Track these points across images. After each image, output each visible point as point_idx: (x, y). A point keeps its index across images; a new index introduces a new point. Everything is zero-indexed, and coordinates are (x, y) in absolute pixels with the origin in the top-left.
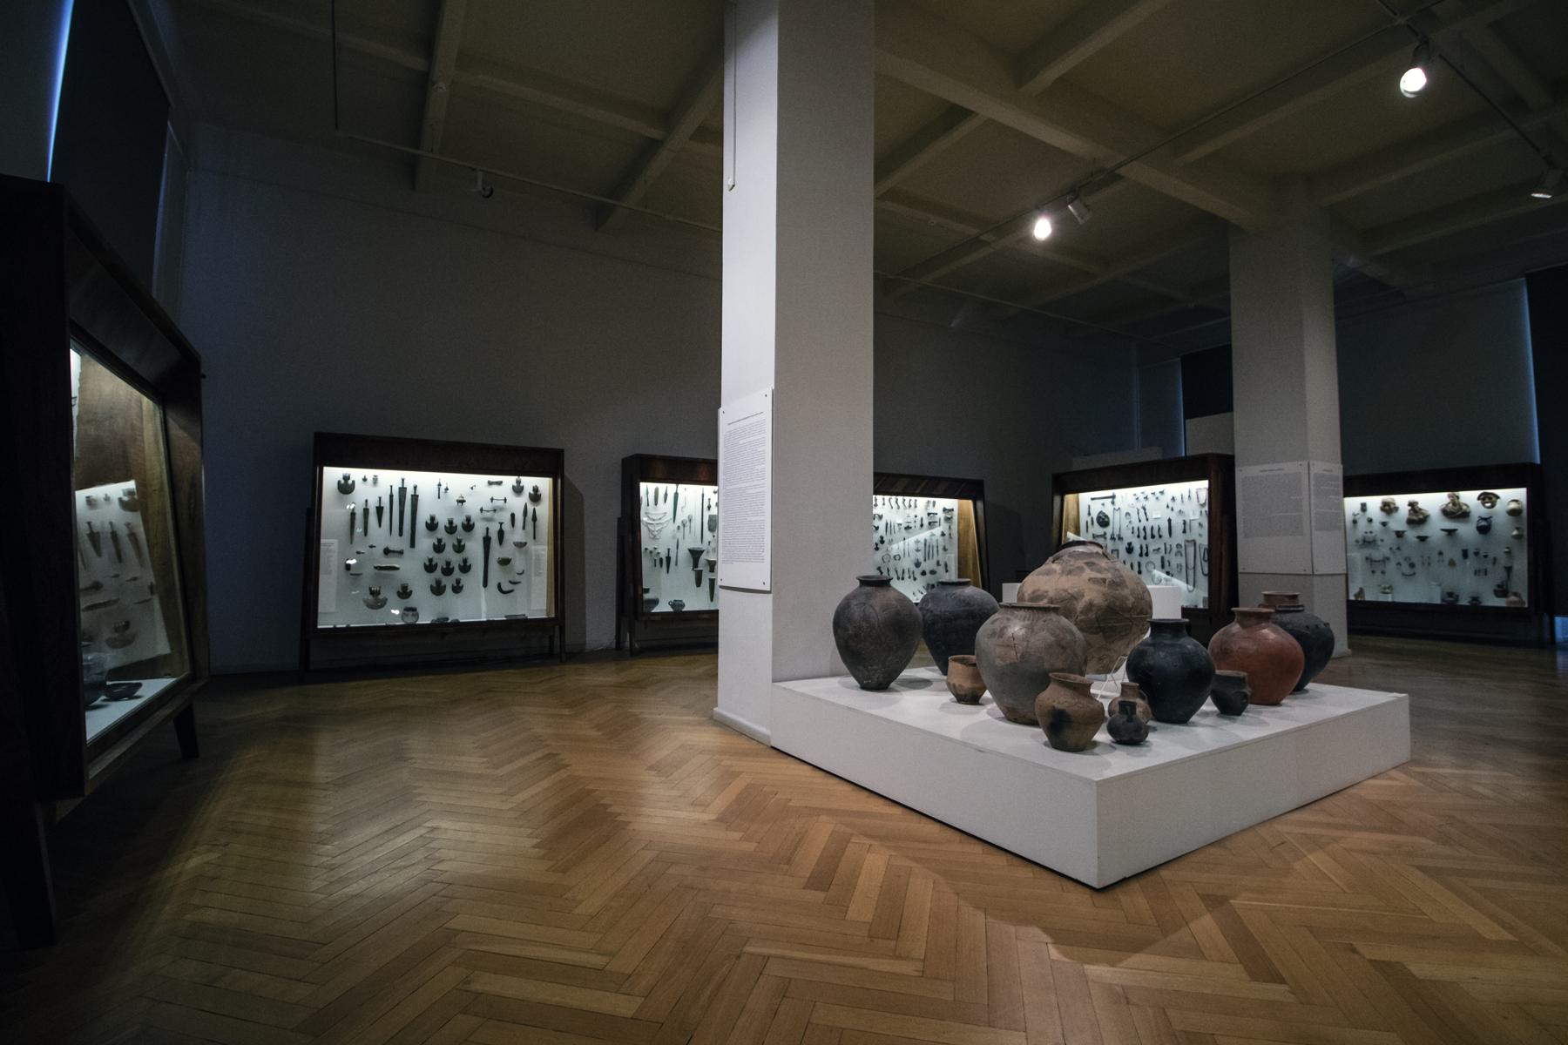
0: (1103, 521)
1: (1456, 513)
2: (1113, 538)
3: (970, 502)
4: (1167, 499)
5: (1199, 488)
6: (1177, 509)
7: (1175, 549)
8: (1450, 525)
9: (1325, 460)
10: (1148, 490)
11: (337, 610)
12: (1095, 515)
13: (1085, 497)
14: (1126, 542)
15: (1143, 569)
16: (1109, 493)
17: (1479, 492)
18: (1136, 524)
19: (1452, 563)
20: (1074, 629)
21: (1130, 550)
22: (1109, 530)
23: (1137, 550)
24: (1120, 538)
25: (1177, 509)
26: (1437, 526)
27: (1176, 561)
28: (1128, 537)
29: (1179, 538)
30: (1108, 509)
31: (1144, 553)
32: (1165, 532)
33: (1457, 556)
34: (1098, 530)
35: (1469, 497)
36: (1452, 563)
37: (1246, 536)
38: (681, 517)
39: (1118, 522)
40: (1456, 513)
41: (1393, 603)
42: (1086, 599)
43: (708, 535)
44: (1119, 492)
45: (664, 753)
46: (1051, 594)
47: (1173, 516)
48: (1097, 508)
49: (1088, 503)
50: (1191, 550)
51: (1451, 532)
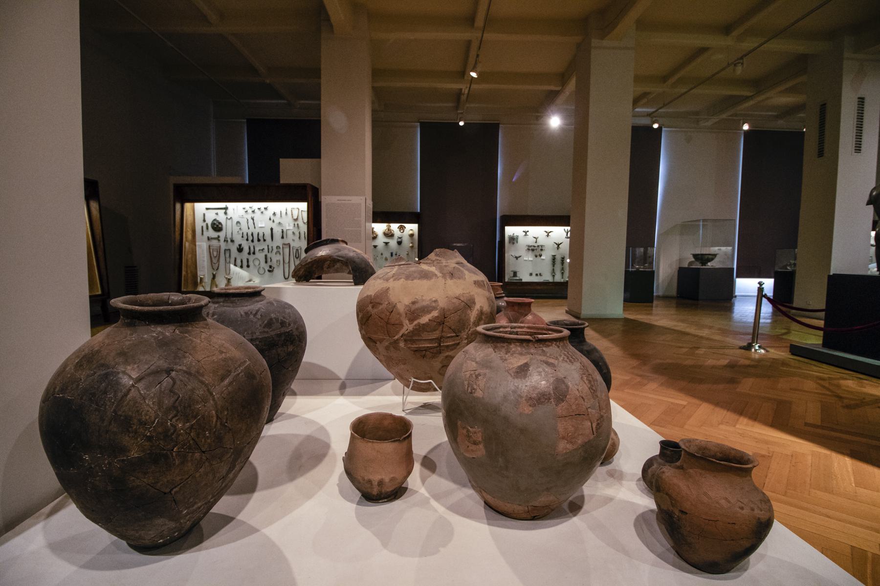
0: (217, 227)
1: (389, 234)
2: (226, 241)
4: (269, 213)
5: (303, 206)
6: (277, 221)
7: (275, 250)
8: (387, 240)
9: (363, 201)
10: (256, 205)
12: (209, 221)
13: (201, 207)
14: (236, 245)
15: (251, 263)
17: (399, 225)
18: (245, 229)
19: (386, 259)
20: (396, 337)
21: (240, 249)
22: (222, 234)
23: (246, 249)
24: (232, 241)
25: (277, 221)
26: (381, 240)
27: (275, 258)
28: (238, 240)
29: (278, 241)
30: (221, 217)
31: (252, 252)
32: (268, 237)
33: (388, 255)
34: (212, 233)
35: (395, 227)
36: (386, 259)
39: (229, 228)
40: (389, 234)
42: (477, 307)
44: (231, 206)
46: (442, 304)
47: (274, 226)
48: (211, 217)
49: (203, 211)
50: (287, 250)
51: (386, 243)
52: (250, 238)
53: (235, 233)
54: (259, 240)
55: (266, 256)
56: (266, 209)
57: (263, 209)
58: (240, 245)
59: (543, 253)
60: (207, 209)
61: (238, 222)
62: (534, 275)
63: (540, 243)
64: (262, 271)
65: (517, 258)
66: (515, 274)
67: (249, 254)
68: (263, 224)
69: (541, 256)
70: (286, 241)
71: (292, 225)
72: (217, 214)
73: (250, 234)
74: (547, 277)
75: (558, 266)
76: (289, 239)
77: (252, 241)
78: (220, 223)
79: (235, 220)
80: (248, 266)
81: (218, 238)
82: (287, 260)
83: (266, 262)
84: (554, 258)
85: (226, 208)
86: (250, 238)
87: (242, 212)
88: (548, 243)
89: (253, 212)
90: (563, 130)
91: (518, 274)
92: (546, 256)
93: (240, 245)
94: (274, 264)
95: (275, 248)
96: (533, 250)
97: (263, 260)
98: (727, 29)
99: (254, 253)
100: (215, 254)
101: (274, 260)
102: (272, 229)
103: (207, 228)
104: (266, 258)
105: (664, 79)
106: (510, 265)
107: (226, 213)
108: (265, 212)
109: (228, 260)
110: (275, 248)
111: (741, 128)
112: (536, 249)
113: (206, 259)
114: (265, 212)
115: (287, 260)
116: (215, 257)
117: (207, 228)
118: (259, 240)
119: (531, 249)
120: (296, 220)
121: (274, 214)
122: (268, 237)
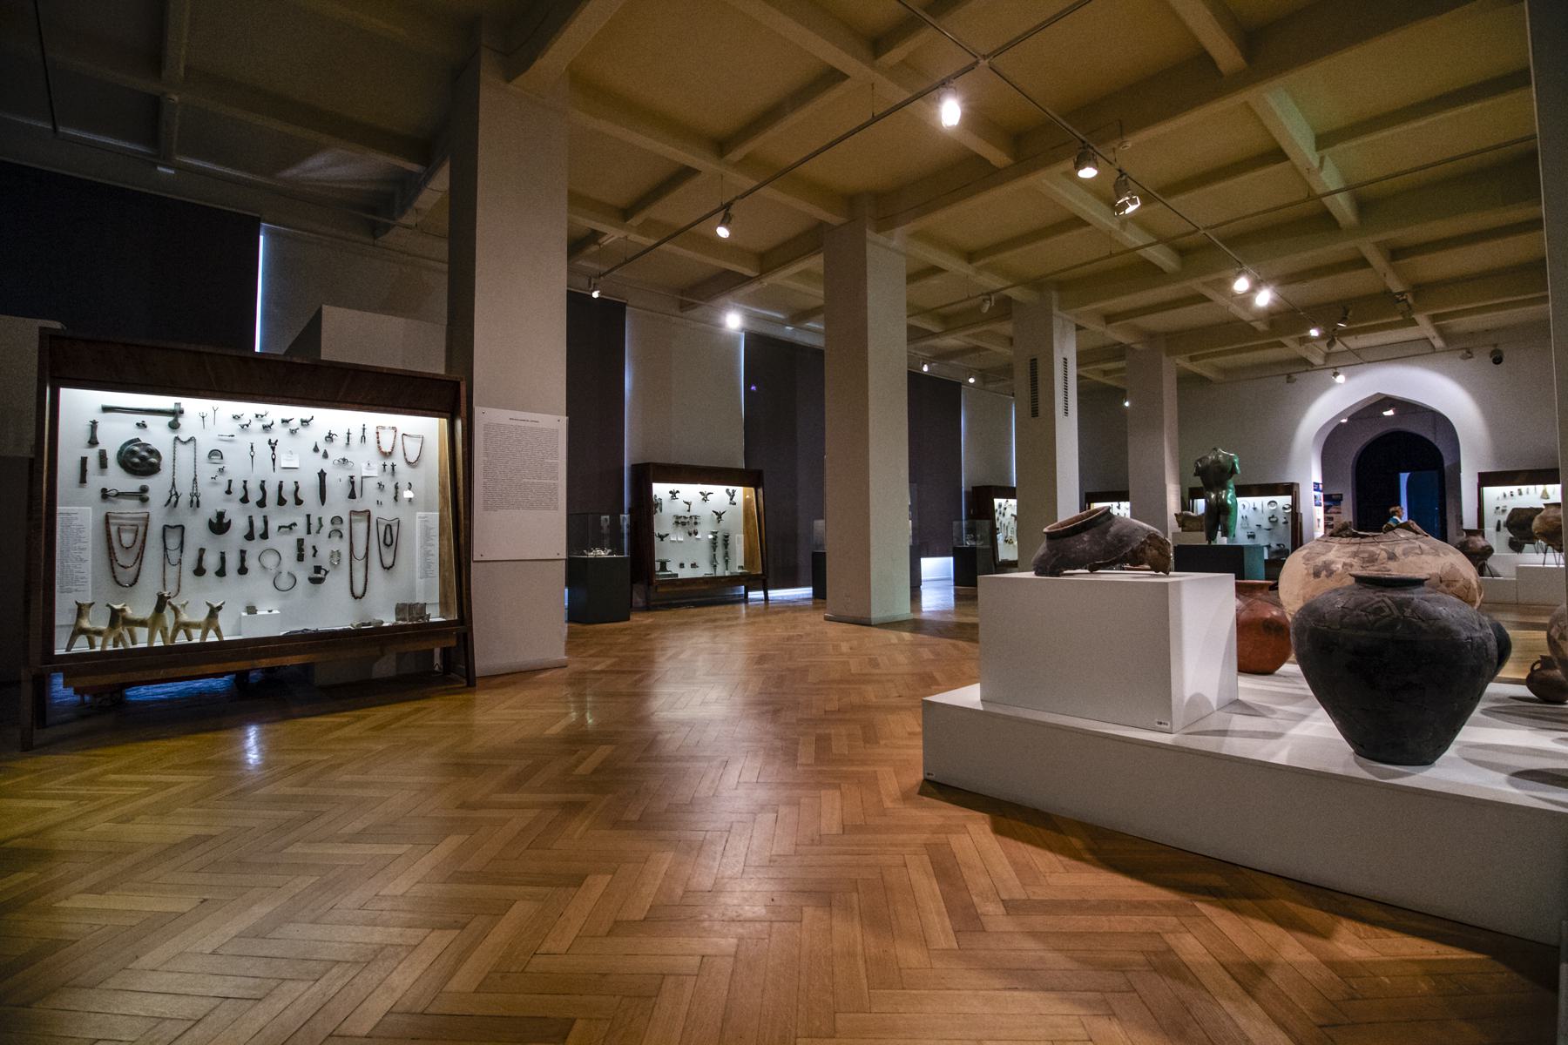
2: (173, 501)
4: (316, 433)
5: (423, 432)
7: (327, 527)
10: (276, 412)
11: (454, 616)
14: (208, 512)
15: (252, 563)
16: (167, 402)
18: (237, 467)
22: (157, 486)
27: (327, 547)
29: (338, 504)
30: (157, 435)
37: (486, 509)
39: (179, 467)
44: (194, 407)
47: (327, 466)
48: (116, 433)
50: (360, 528)
52: (255, 496)
54: (281, 501)
55: (300, 542)
56: (305, 422)
57: (296, 424)
58: (221, 515)
60: (106, 409)
61: (215, 453)
62: (688, 566)
64: (284, 582)
65: (662, 537)
66: (663, 565)
67: (250, 537)
70: (359, 505)
72: (142, 426)
73: (254, 487)
74: (704, 571)
77: (262, 503)
80: (243, 570)
81: (142, 495)
82: (360, 550)
83: (300, 558)
85: (176, 413)
88: (703, 511)
89: (266, 428)
92: (705, 534)
93: (221, 515)
94: (324, 559)
96: (684, 524)
97: (289, 552)
99: (265, 536)
100: (127, 538)
102: (322, 475)
105: (625, 213)
106: (661, 551)
107: (174, 426)
108: (302, 431)
109: (174, 556)
112: (686, 523)
113: (88, 555)
114: (302, 431)
115: (360, 550)
116: (121, 551)
118: (281, 501)
119: (680, 522)
120: (387, 455)
121: (330, 438)
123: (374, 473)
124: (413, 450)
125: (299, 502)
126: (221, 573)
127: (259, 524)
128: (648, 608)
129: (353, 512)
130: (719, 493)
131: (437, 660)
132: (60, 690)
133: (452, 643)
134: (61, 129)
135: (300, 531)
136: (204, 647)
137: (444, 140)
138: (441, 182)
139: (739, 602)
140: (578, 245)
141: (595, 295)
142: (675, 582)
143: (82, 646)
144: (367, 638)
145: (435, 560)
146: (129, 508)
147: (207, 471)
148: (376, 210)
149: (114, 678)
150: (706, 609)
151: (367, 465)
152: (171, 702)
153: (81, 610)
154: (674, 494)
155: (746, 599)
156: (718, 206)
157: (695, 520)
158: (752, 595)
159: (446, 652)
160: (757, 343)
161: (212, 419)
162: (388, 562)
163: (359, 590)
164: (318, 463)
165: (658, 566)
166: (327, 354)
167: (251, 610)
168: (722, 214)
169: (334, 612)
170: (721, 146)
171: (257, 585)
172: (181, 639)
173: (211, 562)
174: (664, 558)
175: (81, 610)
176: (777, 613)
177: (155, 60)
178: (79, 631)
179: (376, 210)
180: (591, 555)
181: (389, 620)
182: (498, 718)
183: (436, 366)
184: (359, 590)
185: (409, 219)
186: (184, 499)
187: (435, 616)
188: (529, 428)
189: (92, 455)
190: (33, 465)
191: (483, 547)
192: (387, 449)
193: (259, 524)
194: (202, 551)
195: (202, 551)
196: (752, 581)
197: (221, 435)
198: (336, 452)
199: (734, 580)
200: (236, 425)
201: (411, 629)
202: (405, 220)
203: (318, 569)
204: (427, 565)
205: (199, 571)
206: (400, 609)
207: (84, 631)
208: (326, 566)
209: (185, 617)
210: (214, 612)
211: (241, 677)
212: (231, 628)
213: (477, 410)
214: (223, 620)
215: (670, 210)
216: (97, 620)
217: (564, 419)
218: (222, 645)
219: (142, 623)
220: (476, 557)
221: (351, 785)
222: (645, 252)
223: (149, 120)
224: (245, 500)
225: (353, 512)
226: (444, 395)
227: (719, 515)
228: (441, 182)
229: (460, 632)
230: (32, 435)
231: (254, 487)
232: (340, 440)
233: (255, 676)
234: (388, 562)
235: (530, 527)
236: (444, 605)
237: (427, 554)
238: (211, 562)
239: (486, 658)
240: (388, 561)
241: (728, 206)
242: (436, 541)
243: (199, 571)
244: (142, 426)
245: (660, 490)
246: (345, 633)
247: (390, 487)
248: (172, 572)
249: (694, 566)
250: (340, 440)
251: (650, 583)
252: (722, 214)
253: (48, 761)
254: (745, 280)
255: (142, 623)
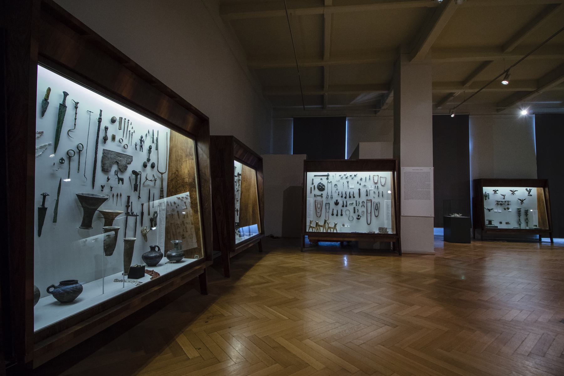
0: (321, 188)
2: (327, 198)
3: (542, 189)
4: (357, 179)
5: (386, 176)
6: (363, 184)
7: (361, 204)
10: (348, 174)
11: (395, 233)
12: (316, 184)
14: (334, 200)
15: (344, 213)
16: (326, 173)
18: (340, 189)
21: (337, 203)
22: (324, 193)
25: (363, 184)
27: (361, 209)
29: (363, 198)
30: (324, 181)
32: (356, 195)
34: (317, 192)
37: (405, 199)
38: (66, 145)
39: (329, 188)
41: (327, 233)
43: (101, 178)
44: (331, 174)
45: (381, 330)
47: (360, 187)
48: (317, 181)
50: (369, 204)
52: (344, 196)
53: (333, 192)
54: (350, 197)
55: (354, 208)
56: (355, 176)
57: (353, 176)
58: (337, 201)
59: (509, 206)
60: (315, 176)
61: (336, 185)
62: (504, 223)
63: (507, 199)
64: (351, 219)
65: (489, 210)
66: (490, 222)
67: (343, 206)
68: (353, 186)
69: (508, 209)
70: (369, 198)
71: (373, 186)
72: (321, 179)
73: (344, 193)
74: (513, 225)
75: (523, 218)
76: (371, 197)
77: (346, 198)
78: (324, 185)
79: (334, 183)
80: (342, 215)
81: (321, 196)
82: (369, 211)
83: (354, 212)
84: (519, 211)
85: (328, 176)
86: (344, 196)
87: (339, 178)
88: (514, 199)
89: (346, 178)
90: (524, 106)
91: (493, 223)
92: (513, 209)
93: (337, 201)
94: (360, 213)
95: (361, 203)
96: (501, 204)
97: (352, 211)
98: (502, 48)
99: (346, 206)
100: (319, 206)
101: (360, 211)
102: (359, 190)
103: (315, 189)
104: (354, 210)
105: (463, 83)
106: (488, 216)
107: (327, 179)
108: (355, 178)
109: (328, 210)
110: (361, 203)
111: (455, 116)
112: (504, 204)
113: (312, 209)
114: (355, 178)
115: (369, 211)
116: (318, 209)
117: (315, 189)
118: (350, 197)
119: (499, 203)
120: (376, 183)
121: (361, 179)
122: (356, 195)
123: (373, 189)
124: (383, 181)
125: (354, 197)
126: (337, 215)
127: (345, 203)
128: (482, 239)
129: (367, 200)
130: (521, 191)
131: (392, 246)
132: (307, 240)
133: (394, 241)
134: (305, 107)
135: (354, 205)
136: (334, 233)
137: (392, 84)
138: (392, 94)
139: (536, 242)
140: (439, 101)
141: (453, 116)
142: (496, 229)
143: (311, 230)
144: (370, 236)
145: (390, 215)
146: (319, 198)
147: (334, 189)
148: (376, 106)
149: (317, 238)
150: (512, 243)
151: (371, 187)
152: (327, 246)
153: (311, 222)
154: (495, 191)
155: (540, 241)
156: (503, 71)
157: (508, 203)
158: (543, 239)
159: (393, 243)
160: (542, 119)
161: (335, 176)
162: (377, 215)
163: (369, 222)
164: (358, 187)
165: (487, 223)
166: (361, 157)
167: (343, 225)
168: (505, 75)
169: (362, 228)
170: (502, 48)
171: (345, 219)
172: (329, 231)
173: (335, 212)
174: (490, 219)
175: (311, 222)
176: (556, 249)
177: (322, 87)
178: (311, 227)
179: (376, 106)
180: (453, 216)
181: (377, 232)
182: (407, 264)
183: (389, 156)
184: (369, 222)
185: (385, 107)
186: (329, 197)
187: (390, 232)
188: (420, 170)
189: (313, 186)
190: (303, 189)
191: (404, 212)
192: (376, 182)
193: (345, 203)
194: (129, 197)
195: (129, 197)
196: (543, 233)
197: (338, 181)
198: (363, 183)
199: (533, 231)
200: (340, 177)
201: (382, 236)
202: (383, 108)
203: (359, 216)
204: (388, 216)
205: (333, 215)
206: (380, 229)
207: (311, 227)
208: (361, 215)
209: (330, 226)
210: (336, 225)
211: (342, 242)
212: (339, 230)
213: (402, 168)
214: (337, 227)
215: (482, 77)
216: (313, 225)
217: (432, 168)
218: (337, 233)
219: (322, 226)
220: (402, 214)
221: (363, 272)
222: (473, 95)
223: (321, 100)
224: (342, 197)
225: (367, 200)
226: (391, 164)
227: (522, 201)
228: (392, 94)
229: (397, 236)
230: (302, 182)
231: (344, 193)
232: (364, 180)
233: (345, 243)
234: (377, 215)
235: (421, 204)
236: (393, 229)
237: (388, 213)
238: (335, 212)
239: (405, 247)
240: (377, 214)
241: (507, 71)
242: (390, 209)
243: (333, 215)
244: (321, 179)
245: (487, 190)
246: (365, 234)
247: (377, 193)
248: (327, 214)
249: (507, 223)
250: (364, 180)
251: (483, 229)
252: (505, 75)
253: (306, 254)
254: (528, 93)
255: (322, 226)
